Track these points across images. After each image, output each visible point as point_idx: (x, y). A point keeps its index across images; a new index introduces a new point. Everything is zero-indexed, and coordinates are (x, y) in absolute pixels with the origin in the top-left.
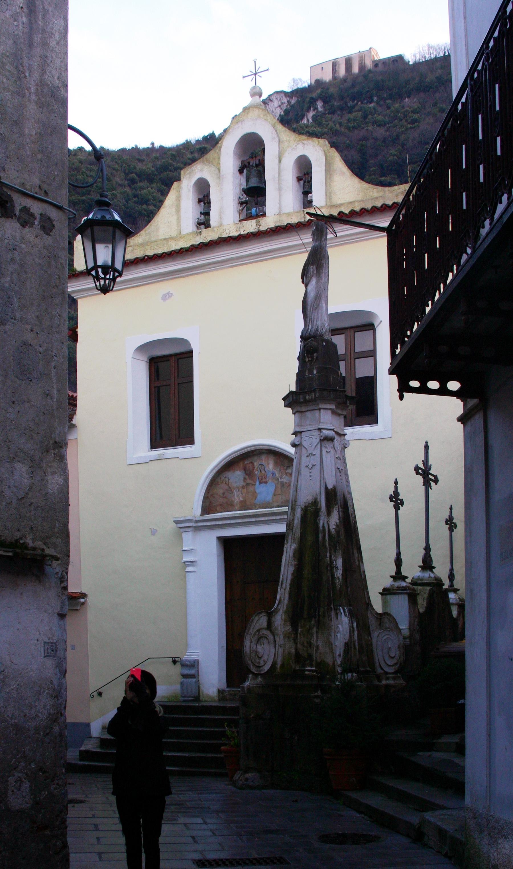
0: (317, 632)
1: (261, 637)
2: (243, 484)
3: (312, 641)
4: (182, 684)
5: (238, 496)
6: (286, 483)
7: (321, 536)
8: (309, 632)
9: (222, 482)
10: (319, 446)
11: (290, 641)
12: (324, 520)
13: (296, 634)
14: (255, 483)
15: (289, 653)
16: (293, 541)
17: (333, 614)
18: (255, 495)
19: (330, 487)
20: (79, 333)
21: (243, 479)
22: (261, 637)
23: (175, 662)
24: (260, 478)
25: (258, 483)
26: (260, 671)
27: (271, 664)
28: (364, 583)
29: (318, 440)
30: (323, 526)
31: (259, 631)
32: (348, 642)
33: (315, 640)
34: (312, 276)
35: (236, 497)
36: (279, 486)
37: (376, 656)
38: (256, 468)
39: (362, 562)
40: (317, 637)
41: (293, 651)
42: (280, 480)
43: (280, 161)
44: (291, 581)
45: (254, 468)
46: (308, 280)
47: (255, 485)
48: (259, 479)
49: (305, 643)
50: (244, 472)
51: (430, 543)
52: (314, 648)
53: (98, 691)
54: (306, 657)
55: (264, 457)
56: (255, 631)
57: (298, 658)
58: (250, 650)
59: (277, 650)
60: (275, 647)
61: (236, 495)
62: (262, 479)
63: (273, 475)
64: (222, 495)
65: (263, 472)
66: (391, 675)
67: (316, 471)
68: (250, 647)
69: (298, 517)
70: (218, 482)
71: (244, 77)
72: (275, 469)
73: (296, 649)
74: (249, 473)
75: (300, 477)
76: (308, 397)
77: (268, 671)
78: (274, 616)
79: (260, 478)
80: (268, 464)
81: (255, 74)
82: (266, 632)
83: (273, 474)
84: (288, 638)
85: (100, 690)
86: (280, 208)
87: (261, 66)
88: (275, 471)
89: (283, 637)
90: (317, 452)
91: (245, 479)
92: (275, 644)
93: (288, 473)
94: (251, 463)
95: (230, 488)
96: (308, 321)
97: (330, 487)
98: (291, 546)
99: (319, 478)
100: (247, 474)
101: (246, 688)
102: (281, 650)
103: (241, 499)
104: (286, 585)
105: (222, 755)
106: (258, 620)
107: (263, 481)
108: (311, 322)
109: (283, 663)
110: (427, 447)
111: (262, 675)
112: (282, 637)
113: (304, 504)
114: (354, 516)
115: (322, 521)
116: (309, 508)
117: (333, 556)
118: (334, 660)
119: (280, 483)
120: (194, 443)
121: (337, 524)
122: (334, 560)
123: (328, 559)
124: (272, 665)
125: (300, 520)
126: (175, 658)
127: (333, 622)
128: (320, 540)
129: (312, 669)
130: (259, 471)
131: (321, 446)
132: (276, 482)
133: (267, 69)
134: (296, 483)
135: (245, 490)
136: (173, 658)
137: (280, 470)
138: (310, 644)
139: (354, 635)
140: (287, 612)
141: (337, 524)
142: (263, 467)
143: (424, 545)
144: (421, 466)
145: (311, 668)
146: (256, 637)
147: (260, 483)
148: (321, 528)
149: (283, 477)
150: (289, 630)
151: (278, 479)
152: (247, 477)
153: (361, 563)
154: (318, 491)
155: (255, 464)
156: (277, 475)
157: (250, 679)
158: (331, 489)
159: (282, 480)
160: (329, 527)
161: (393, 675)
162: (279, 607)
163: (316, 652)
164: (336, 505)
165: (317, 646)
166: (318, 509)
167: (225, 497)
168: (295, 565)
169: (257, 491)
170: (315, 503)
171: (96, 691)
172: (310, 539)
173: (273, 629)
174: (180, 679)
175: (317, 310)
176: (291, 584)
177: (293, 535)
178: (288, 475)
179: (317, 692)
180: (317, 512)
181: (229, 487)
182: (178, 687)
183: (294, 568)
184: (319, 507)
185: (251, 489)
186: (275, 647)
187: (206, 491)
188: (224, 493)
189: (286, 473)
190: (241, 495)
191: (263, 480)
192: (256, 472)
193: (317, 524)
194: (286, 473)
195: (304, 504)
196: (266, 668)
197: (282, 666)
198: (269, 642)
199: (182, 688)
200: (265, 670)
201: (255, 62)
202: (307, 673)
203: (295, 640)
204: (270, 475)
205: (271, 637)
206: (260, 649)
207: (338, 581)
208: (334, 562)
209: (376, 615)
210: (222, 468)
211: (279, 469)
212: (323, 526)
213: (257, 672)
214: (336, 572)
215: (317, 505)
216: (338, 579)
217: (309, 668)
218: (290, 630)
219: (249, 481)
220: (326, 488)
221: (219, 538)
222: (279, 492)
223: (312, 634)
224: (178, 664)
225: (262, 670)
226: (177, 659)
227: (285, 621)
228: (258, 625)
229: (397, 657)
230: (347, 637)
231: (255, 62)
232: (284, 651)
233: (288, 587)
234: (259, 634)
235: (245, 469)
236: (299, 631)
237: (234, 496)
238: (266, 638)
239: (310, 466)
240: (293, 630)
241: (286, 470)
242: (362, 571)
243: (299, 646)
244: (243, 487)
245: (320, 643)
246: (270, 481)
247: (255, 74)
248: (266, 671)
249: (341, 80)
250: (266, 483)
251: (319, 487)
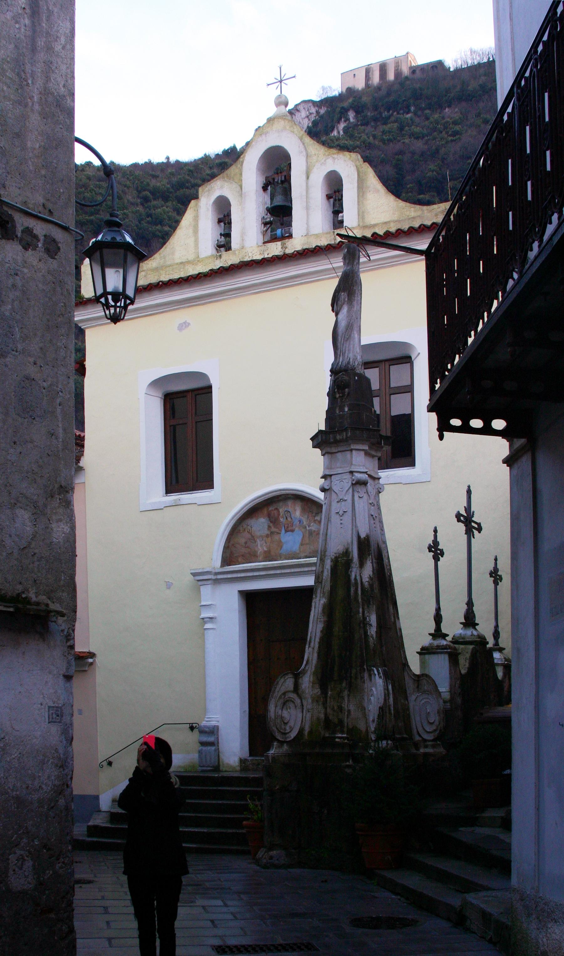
0: (349, 696)
1: (287, 701)
2: (267, 532)
3: (343, 706)
4: (200, 752)
5: (261, 546)
6: (314, 531)
7: (352, 590)
8: (339, 695)
9: (244, 530)
10: (351, 490)
11: (319, 705)
12: (356, 572)
13: (326, 697)
14: (281, 531)
15: (318, 719)
16: (322, 595)
17: (366, 675)
18: (280, 544)
19: (363, 536)
20: (86, 366)
21: (267, 527)
22: (287, 701)
23: (192, 728)
24: (286, 526)
25: (283, 531)
26: (286, 738)
27: (298, 730)
28: (400, 641)
29: (350, 484)
30: (355, 579)
31: (284, 694)
32: (382, 706)
33: (346, 704)
34: (344, 304)
35: (259, 547)
36: (307, 535)
37: (414, 722)
38: (281, 515)
39: (398, 618)
40: (349, 701)
41: (322, 716)
42: (308, 528)
43: (308, 178)
44: (320, 639)
45: (279, 515)
46: (339, 308)
47: (280, 533)
48: (284, 527)
49: (336, 708)
50: (268, 519)
51: (473, 597)
52: (345, 713)
53: (107, 760)
54: (337, 722)
55: (290, 503)
56: (280, 694)
57: (327, 723)
58: (275, 715)
59: (304, 715)
60: (303, 712)
61: (259, 545)
62: (288, 527)
63: (300, 523)
64: (244, 545)
65: (289, 519)
66: (430, 743)
67: (347, 518)
68: (275, 711)
69: (327, 569)
70: (240, 530)
71: (268, 85)
72: (302, 516)
73: (326, 714)
74: (274, 521)
75: (329, 524)
76: (338, 437)
77: (295, 738)
78: (302, 677)
79: (286, 526)
80: (295, 510)
81: (281, 82)
82: (293, 696)
83: (300, 521)
84: (317, 701)
85: (110, 759)
86: (308, 229)
87: (287, 72)
88: (303, 518)
89: (311, 701)
90: (349, 497)
91: (269, 527)
92: (303, 709)
93: (317, 520)
94: (276, 509)
95: (253, 537)
96: (339, 353)
97: (363, 536)
98: (320, 600)
99: (350, 526)
100: (271, 522)
101: (270, 757)
102: (309, 716)
103: (265, 549)
104: (314, 643)
105: (244, 831)
106: (284, 682)
107: (289, 529)
108: (341, 354)
109: (311, 729)
110: (469, 492)
111: (288, 743)
112: (310, 701)
113: (334, 554)
114: (389, 567)
115: (354, 573)
116: (339, 559)
117: (366, 612)
118: (367, 726)
119: (308, 532)
120: (213, 488)
121: (370, 576)
122: (368, 616)
123: (361, 614)
124: (299, 732)
125: (330, 572)
126: (192, 723)
127: (366, 684)
128: (352, 594)
129: (343, 736)
130: (285, 518)
131: (353, 491)
132: (303, 530)
133: (293, 76)
134: (325, 531)
135: (270, 539)
136: (190, 724)
137: (308, 517)
138: (341, 709)
139: (389, 698)
140: (315, 673)
141: (370, 576)
142: (289, 514)
143: (466, 599)
144: (463, 512)
145: (342, 734)
146: (282, 701)
147: (286, 531)
148: (353, 581)
149: (312, 524)
150: (317, 693)
151: (306, 527)
152: (271, 525)
153: (397, 620)
154: (350, 541)
155: (281, 510)
156: (305, 523)
157: (275, 747)
158: (364, 538)
159: (310, 528)
160: (361, 580)
161: (433, 743)
162: (307, 668)
163: (347, 718)
164: (369, 555)
165: (349, 711)
166: (350, 560)
167: (248, 547)
168: (325, 622)
169: (283, 540)
170: (347, 553)
171: (106, 760)
172: (341, 593)
173: (300, 692)
174: (198, 747)
175: (348, 341)
176: (319, 643)
177: (322, 589)
178: (317, 522)
179: (349, 761)
180: (348, 564)
181: (252, 536)
182: (196, 756)
183: (323, 625)
184: (350, 558)
185: (276, 537)
186: (303, 712)
187: (227, 540)
188: (246, 543)
189: (315, 521)
190: (264, 544)
191: (289, 529)
192: (282, 520)
193: (349, 577)
194: (315, 521)
195: (334, 554)
196: (293, 735)
197: (310, 732)
198: (296, 707)
199: (200, 757)
200: (291, 737)
201: (280, 68)
202: (337, 740)
203: (324, 704)
204: (296, 522)
205: (298, 701)
206: (285, 714)
207: (371, 639)
208: (368, 618)
209: (413, 677)
210: (244, 514)
211: (306, 516)
212: (355, 579)
213: (282, 740)
214: (369, 629)
215: (349, 556)
216: (372, 637)
217: (340, 735)
218: (319, 693)
219: (273, 529)
220: (359, 537)
221: (241, 592)
222: (307, 541)
223: (343, 698)
224: (196, 731)
225: (288, 737)
226: (194, 725)
227: (313, 683)
228: (283, 687)
229: (437, 723)
230: (382, 701)
231: (280, 68)
232: (312, 717)
233: (317, 646)
234: (284, 697)
235: (269, 516)
236: (329, 695)
237: (257, 545)
238: (293, 702)
239: (341, 513)
240: (322, 693)
241: (315, 517)
242: (398, 628)
243: (329, 710)
244: (267, 536)
245: (352, 708)
246: (297, 529)
247: (281, 82)
248: (292, 738)
249: (375, 88)
250: (292, 531)
251: (350, 536)
